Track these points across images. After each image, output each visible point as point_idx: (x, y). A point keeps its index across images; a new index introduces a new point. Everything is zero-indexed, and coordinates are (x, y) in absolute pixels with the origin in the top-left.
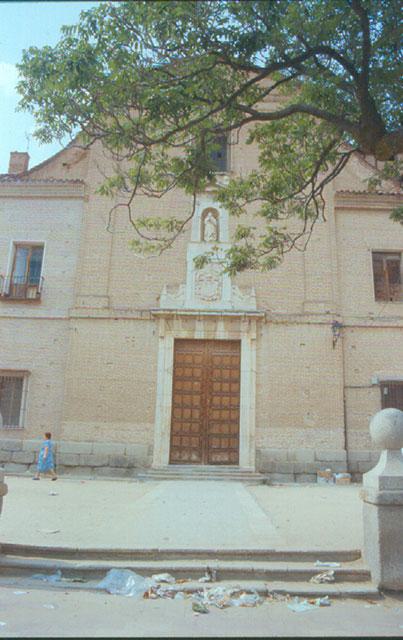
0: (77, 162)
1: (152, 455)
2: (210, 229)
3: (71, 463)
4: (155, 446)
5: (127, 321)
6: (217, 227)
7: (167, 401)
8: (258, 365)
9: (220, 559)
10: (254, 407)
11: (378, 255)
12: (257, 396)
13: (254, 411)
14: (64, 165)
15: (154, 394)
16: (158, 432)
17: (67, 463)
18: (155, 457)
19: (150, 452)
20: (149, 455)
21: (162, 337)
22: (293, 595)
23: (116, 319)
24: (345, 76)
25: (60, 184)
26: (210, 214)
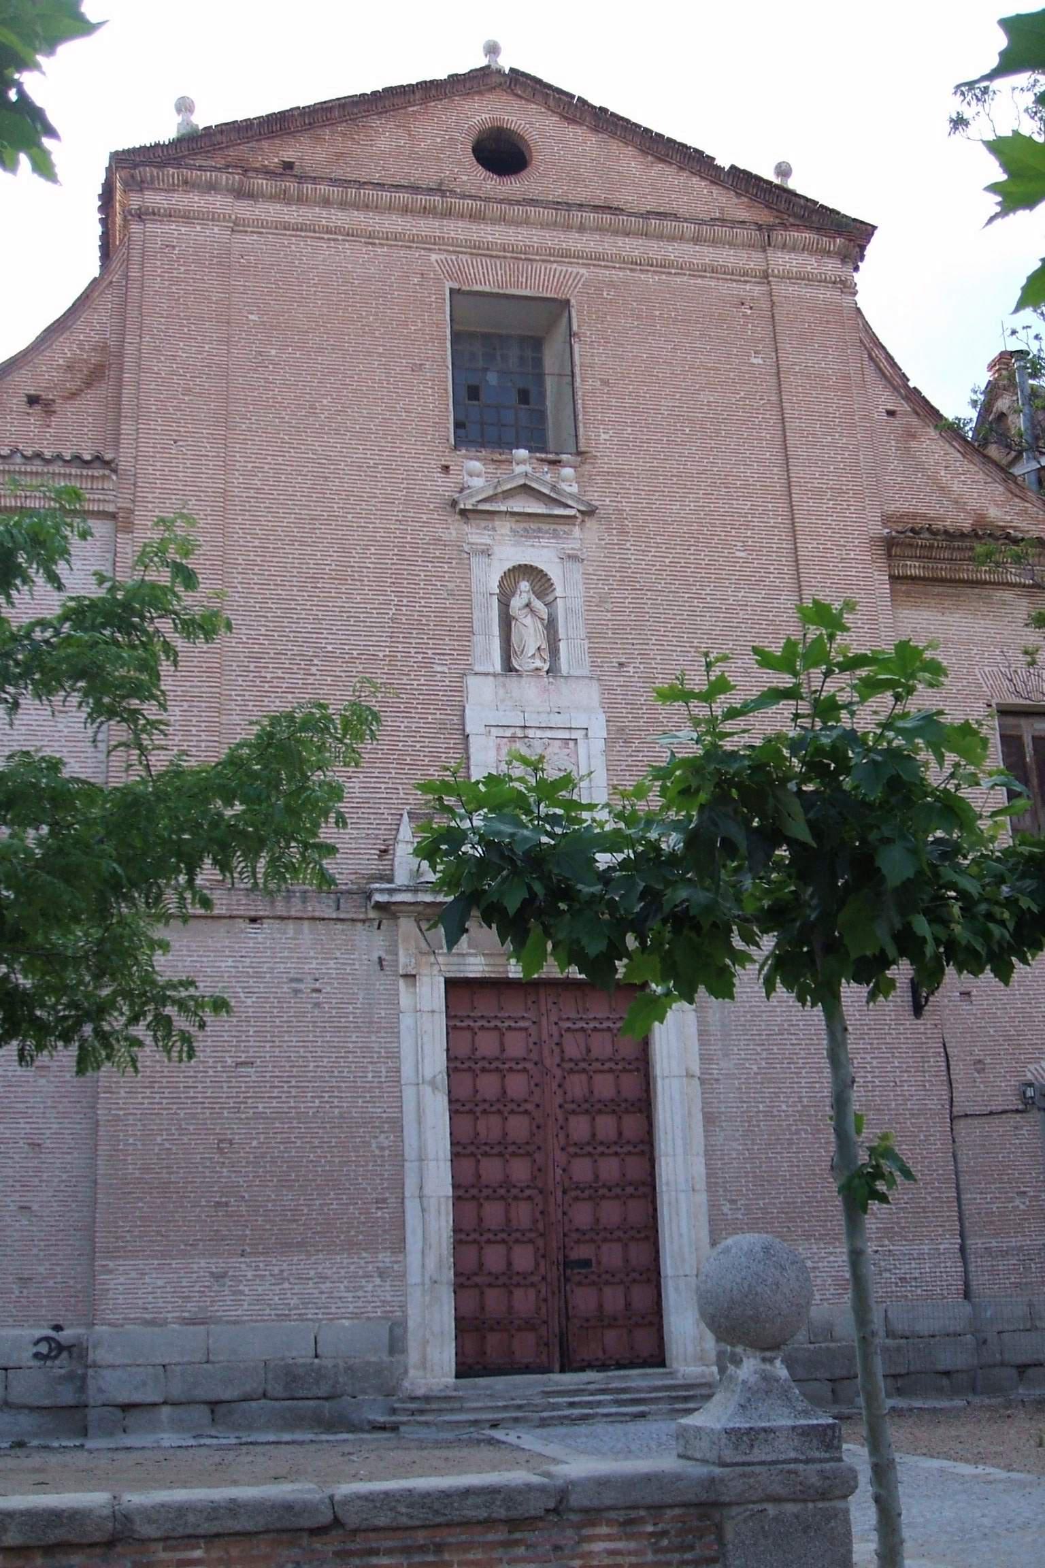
0: (73, 395)
1: (404, 1351)
2: (530, 634)
3: (137, 1398)
4: (411, 1324)
5: (291, 927)
6: (551, 626)
7: (441, 1224)
8: (705, 1059)
9: (598, 1371)
10: (701, 1184)
11: (1011, 721)
12: (709, 1153)
13: (702, 1198)
14: (33, 400)
15: (398, 1158)
16: (414, 1277)
17: (124, 1397)
18: (413, 1356)
19: (396, 1344)
20: (392, 1350)
21: (410, 977)
22: (350, 234)
23: (253, 920)
24: (32, 1037)
25: (37, 467)
26: (524, 585)
